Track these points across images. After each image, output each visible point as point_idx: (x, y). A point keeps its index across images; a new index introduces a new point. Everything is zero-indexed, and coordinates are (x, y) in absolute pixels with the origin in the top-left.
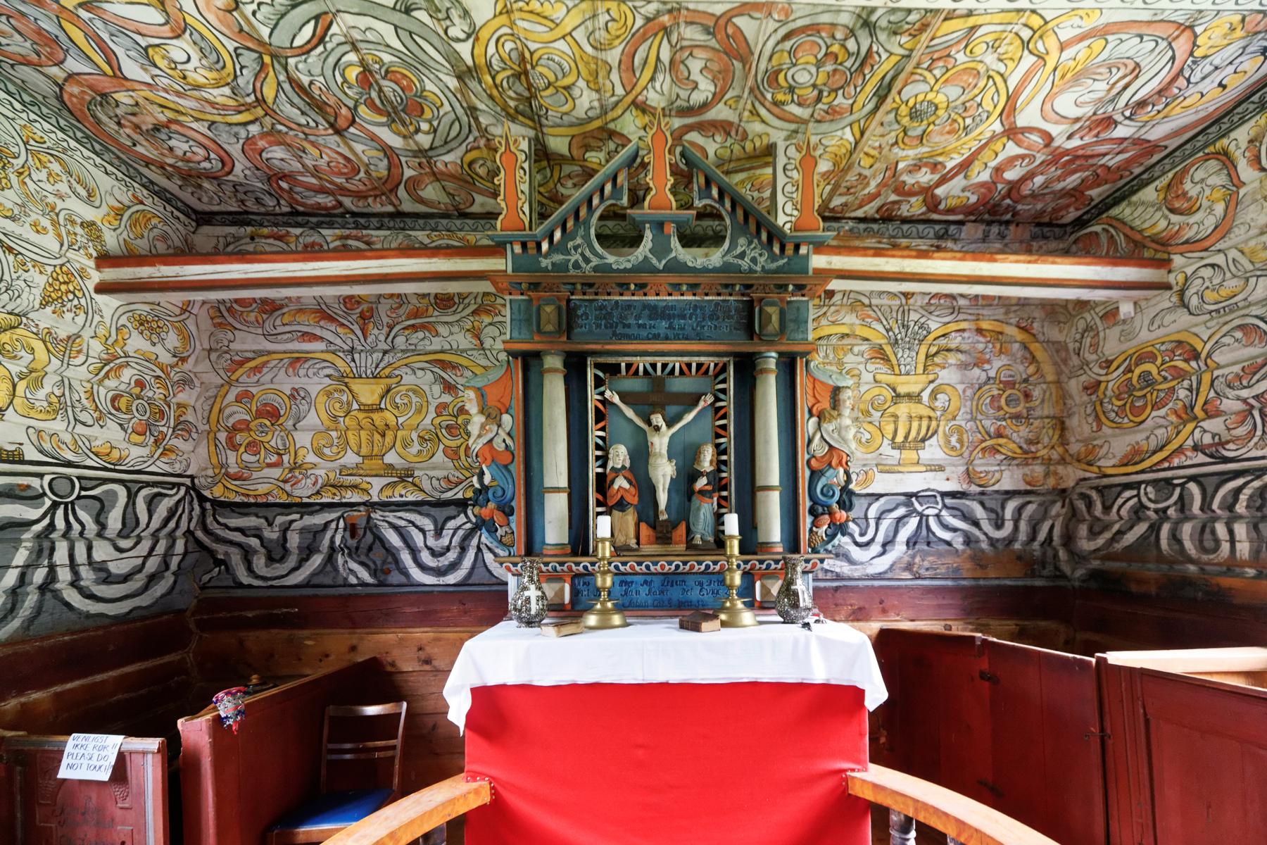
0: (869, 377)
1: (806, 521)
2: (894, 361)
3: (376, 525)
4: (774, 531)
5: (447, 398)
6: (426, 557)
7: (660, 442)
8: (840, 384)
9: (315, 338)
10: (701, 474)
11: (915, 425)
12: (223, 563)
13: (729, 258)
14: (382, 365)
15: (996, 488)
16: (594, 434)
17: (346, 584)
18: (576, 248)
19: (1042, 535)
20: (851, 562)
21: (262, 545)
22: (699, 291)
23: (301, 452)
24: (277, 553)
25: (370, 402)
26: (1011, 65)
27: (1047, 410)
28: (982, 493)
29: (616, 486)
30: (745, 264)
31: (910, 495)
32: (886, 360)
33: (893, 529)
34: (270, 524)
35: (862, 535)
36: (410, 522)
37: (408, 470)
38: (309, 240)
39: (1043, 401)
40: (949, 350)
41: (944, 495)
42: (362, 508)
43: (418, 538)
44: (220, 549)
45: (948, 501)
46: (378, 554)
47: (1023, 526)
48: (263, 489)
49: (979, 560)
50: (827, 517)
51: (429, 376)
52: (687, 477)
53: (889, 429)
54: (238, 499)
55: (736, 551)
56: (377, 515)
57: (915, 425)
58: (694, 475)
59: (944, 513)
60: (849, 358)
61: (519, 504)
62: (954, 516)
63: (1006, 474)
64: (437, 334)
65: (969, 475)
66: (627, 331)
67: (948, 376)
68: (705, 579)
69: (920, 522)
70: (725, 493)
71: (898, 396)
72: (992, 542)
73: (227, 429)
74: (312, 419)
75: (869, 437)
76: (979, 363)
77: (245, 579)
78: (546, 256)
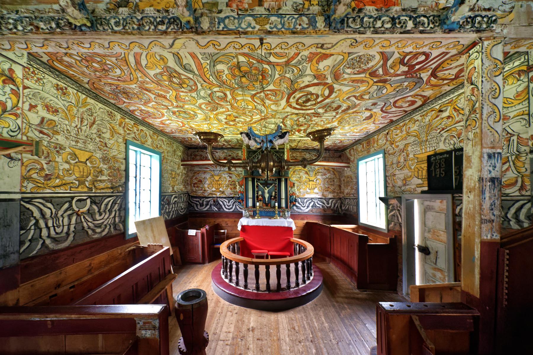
4: (283, 205)
6: (227, 206)
7: (266, 191)
9: (208, 168)
16: (256, 189)
19: (336, 206)
24: (202, 205)
27: (338, 184)
32: (308, 174)
44: (192, 204)
46: (218, 206)
48: (199, 194)
49: (324, 210)
52: (271, 196)
53: (308, 186)
56: (218, 199)
60: (301, 174)
61: (245, 200)
65: (323, 195)
67: (319, 177)
74: (207, 182)
76: (325, 175)
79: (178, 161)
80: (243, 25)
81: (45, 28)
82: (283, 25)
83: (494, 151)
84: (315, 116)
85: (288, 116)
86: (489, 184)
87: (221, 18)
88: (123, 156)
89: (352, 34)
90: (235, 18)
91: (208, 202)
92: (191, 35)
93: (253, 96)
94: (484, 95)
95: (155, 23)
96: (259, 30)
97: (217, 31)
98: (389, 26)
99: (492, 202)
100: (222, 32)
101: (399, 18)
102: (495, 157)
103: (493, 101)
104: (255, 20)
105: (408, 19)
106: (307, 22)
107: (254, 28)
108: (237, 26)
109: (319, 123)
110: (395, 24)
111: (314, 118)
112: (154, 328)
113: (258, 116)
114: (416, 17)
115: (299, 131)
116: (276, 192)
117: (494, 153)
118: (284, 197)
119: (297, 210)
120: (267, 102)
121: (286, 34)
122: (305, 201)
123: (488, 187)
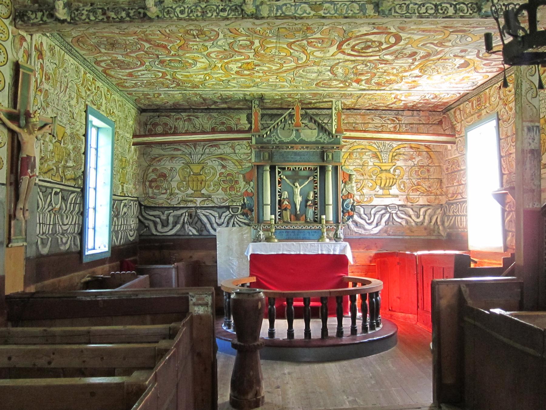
0: (372, 164)
2: (380, 158)
3: (199, 215)
5: (223, 171)
7: (298, 191)
8: (351, 173)
9: (179, 150)
10: (309, 200)
11: (388, 181)
13: (318, 139)
14: (201, 159)
15: (417, 203)
16: (278, 188)
17: (189, 235)
18: (274, 136)
20: (365, 229)
21: (161, 221)
22: (309, 148)
23: (173, 189)
24: (165, 224)
25: (197, 172)
26: (282, 222)
28: (412, 205)
29: (284, 204)
30: (322, 140)
31: (387, 206)
32: (378, 157)
33: (380, 218)
34: (163, 214)
35: (369, 220)
36: (210, 213)
37: (209, 195)
38: (177, 117)
39: (434, 173)
40: (400, 154)
41: (399, 206)
42: (193, 209)
43: (213, 219)
44: (146, 222)
45: (400, 208)
46: (199, 224)
47: (427, 217)
48: (161, 201)
50: (347, 213)
51: (217, 163)
54: (153, 205)
55: (324, 223)
56: (199, 211)
57: (388, 181)
58: (307, 201)
59: (398, 212)
60: (365, 157)
62: (402, 214)
63: (421, 199)
64: (220, 148)
66: (288, 159)
67: (399, 163)
68: (310, 231)
69: (390, 216)
70: (316, 206)
71: (382, 170)
72: (416, 223)
73: (149, 181)
74: (177, 178)
75: (371, 185)
76: (411, 159)
77: (154, 232)
78: (265, 138)
79: (129, 136)
80: (299, 12)
81: (115, 17)
82: (336, 11)
83: (533, 124)
84: (381, 64)
85: (339, 63)
86: (529, 155)
87: (279, 6)
88: (83, 131)
89: (399, 18)
90: (291, 6)
92: (251, 20)
93: (290, 45)
94: (522, 72)
95: (218, 10)
96: (314, 15)
97: (275, 16)
98: (432, 11)
99: (532, 172)
100: (280, 18)
101: (440, 5)
102: (533, 130)
103: (530, 78)
104: (311, 7)
105: (448, 6)
106: (358, 8)
107: (310, 13)
108: (294, 12)
109: (391, 71)
110: (438, 10)
111: (380, 66)
112: (206, 305)
113: (293, 64)
114: (456, 4)
115: (358, 81)
116: (315, 193)
117: (533, 127)
118: (331, 202)
119: (356, 229)
120: (310, 49)
121: (339, 18)
122: (373, 212)
123: (529, 159)
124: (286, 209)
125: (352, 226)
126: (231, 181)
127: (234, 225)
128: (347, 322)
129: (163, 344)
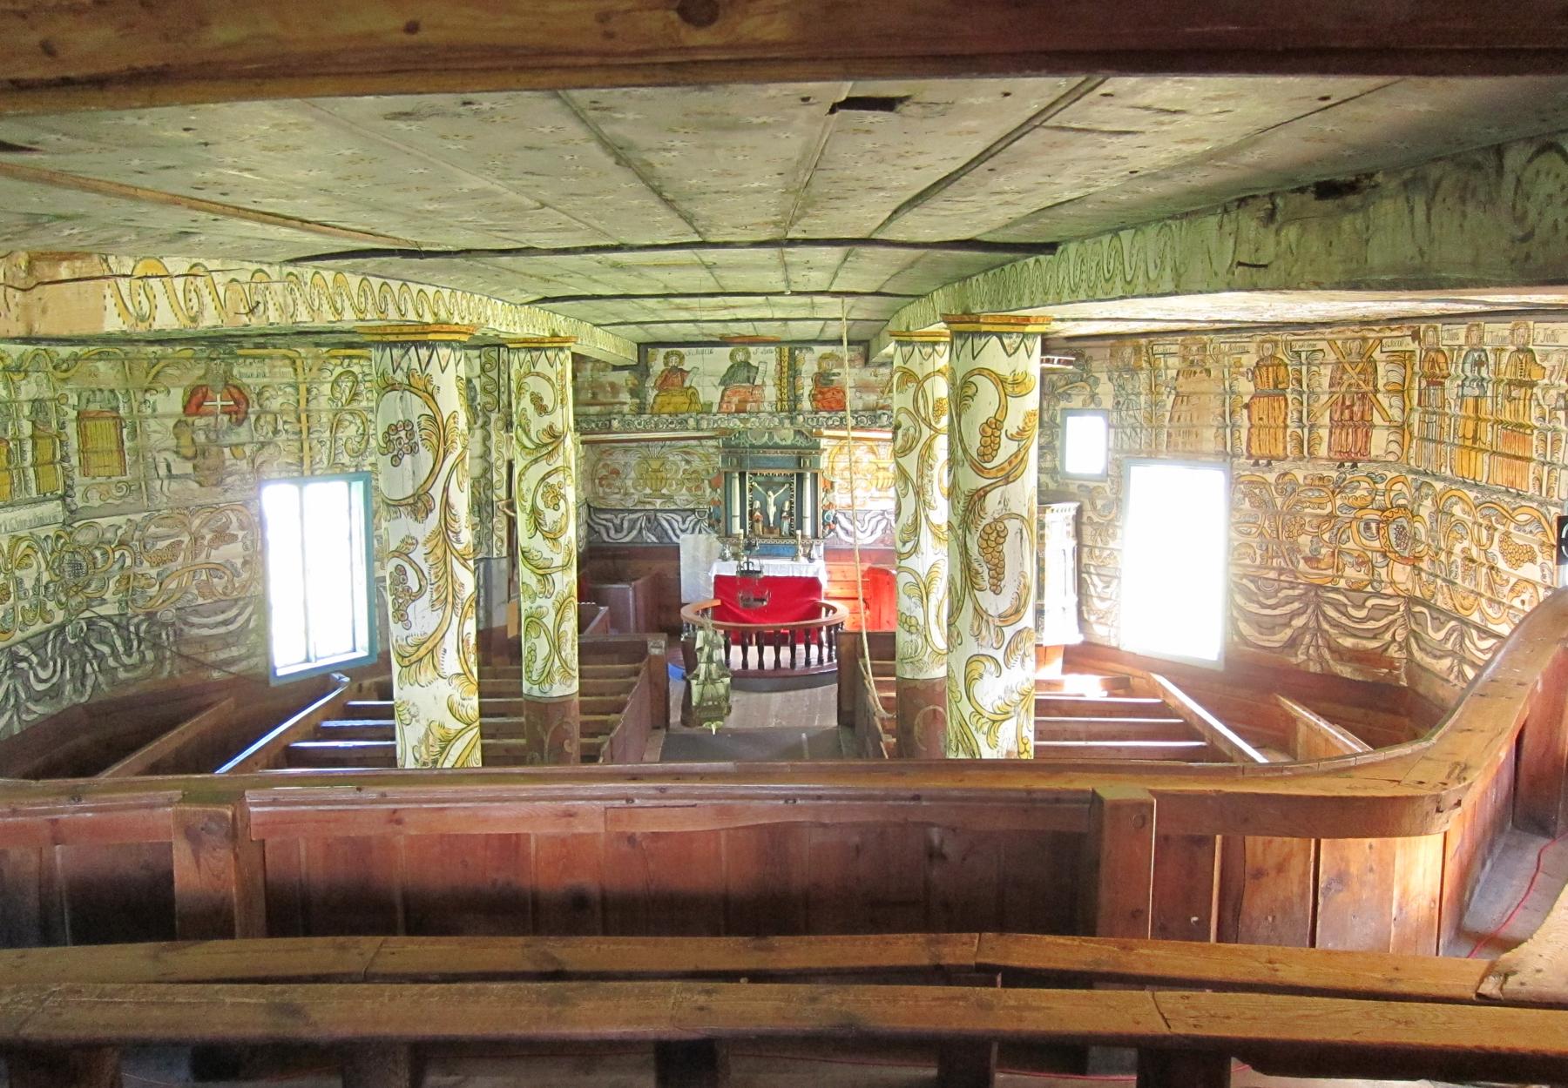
1: (821, 528)
12: (598, 532)
24: (619, 529)
32: (874, 453)
52: (780, 511)
53: (875, 482)
56: (659, 514)
58: (782, 511)
61: (723, 519)
74: (633, 475)
77: (607, 539)
91: (635, 522)
116: (791, 503)
122: (867, 518)
124: (758, 521)
125: (841, 533)
126: (697, 479)
127: (700, 532)
128: (814, 649)
129: (633, 679)
